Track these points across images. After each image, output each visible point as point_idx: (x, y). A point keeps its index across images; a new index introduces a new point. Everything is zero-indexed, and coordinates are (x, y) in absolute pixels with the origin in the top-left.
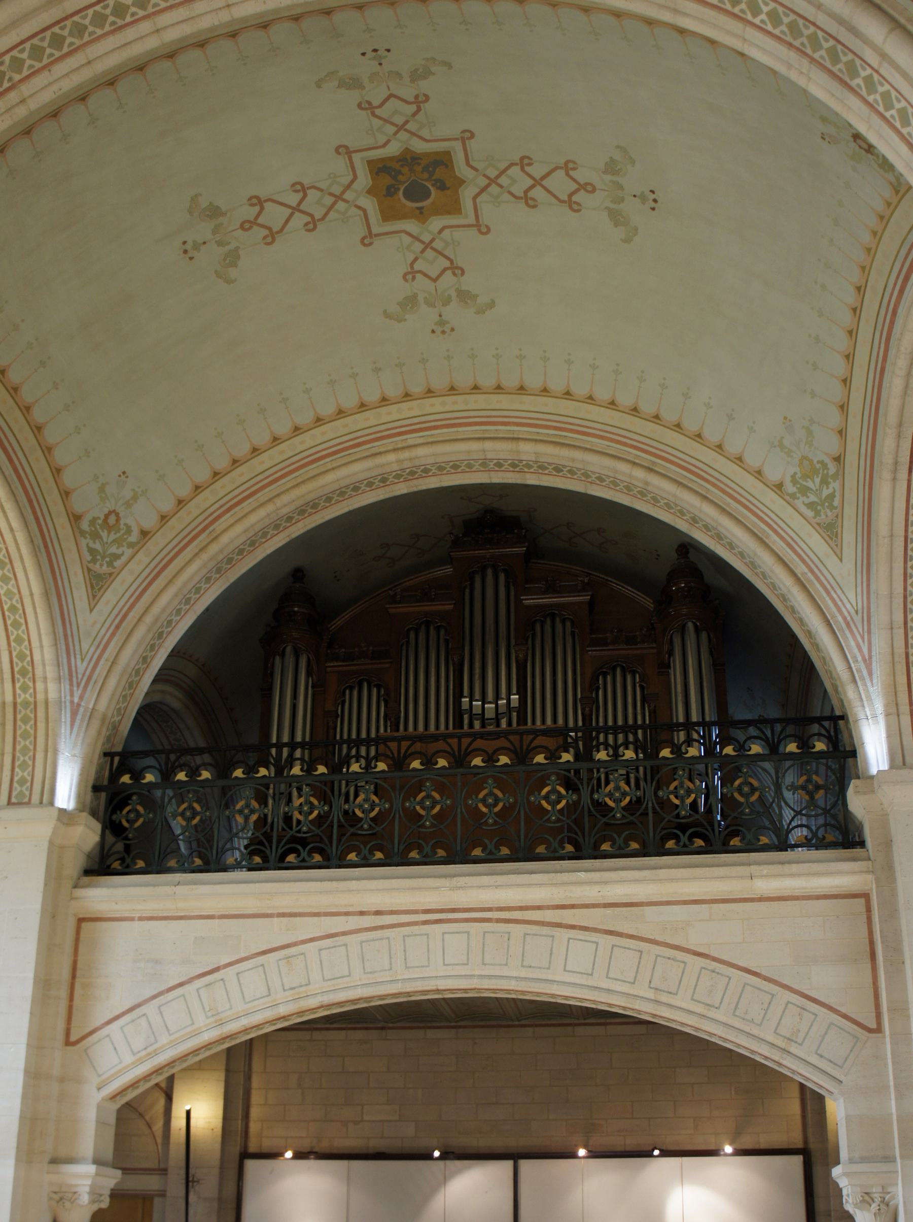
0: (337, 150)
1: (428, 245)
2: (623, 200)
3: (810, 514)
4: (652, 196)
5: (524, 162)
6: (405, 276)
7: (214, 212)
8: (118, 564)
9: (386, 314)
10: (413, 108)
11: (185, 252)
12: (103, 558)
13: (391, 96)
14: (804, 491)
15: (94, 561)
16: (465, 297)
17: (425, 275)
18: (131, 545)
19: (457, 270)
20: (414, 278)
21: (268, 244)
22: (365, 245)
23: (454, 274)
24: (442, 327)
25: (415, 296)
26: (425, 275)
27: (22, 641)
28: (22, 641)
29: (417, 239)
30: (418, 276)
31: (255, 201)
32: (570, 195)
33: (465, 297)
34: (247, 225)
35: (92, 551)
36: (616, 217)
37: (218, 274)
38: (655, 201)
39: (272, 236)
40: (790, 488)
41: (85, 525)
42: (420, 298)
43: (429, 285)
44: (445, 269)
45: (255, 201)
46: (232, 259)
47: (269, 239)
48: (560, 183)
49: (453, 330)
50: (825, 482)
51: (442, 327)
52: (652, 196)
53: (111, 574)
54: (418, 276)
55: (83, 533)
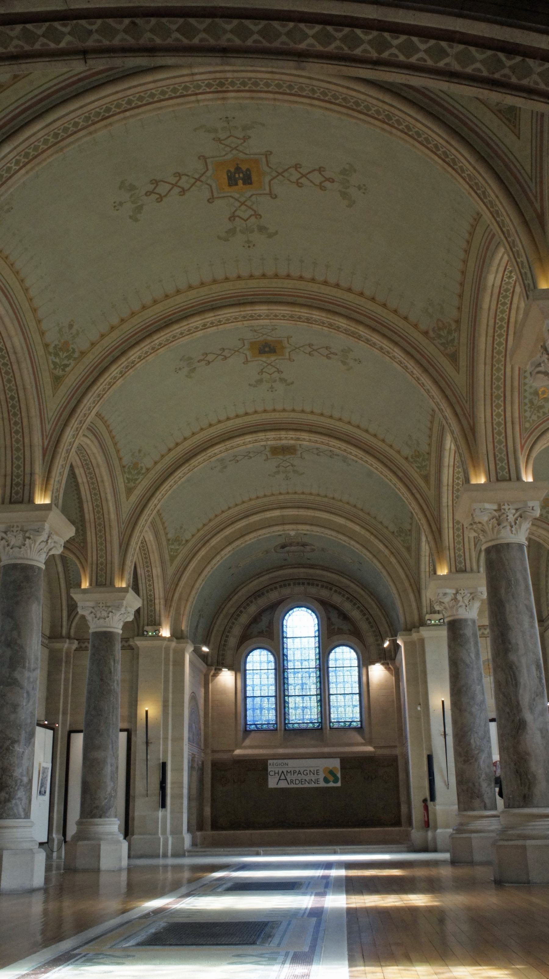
0: (199, 158)
1: (243, 204)
2: (349, 187)
3: (442, 348)
4: (364, 188)
5: (297, 167)
6: (230, 219)
7: (132, 188)
8: (67, 369)
9: (219, 237)
10: (242, 141)
11: (115, 207)
12: (60, 367)
13: (246, 220)
14: (440, 336)
15: (55, 368)
16: (262, 229)
17: (240, 218)
18: (75, 359)
19: (257, 215)
20: (234, 220)
21: (158, 202)
22: (211, 203)
23: (256, 218)
24: (249, 244)
25: (235, 228)
26: (240, 218)
27: (457, 536)
28: (457, 536)
29: (236, 200)
30: (237, 219)
31: (154, 182)
32: (321, 183)
33: (262, 229)
34: (148, 194)
35: (54, 363)
36: (344, 195)
37: (131, 217)
38: (365, 189)
39: (161, 198)
40: (431, 334)
41: (51, 349)
42: (238, 229)
43: (268, 376)
44: (251, 216)
45: (154, 182)
46: (139, 209)
47: (159, 200)
48: (317, 178)
49: (254, 245)
50: (450, 332)
51: (287, 478)
52: (364, 188)
53: (64, 376)
54: (237, 219)
55: (50, 354)
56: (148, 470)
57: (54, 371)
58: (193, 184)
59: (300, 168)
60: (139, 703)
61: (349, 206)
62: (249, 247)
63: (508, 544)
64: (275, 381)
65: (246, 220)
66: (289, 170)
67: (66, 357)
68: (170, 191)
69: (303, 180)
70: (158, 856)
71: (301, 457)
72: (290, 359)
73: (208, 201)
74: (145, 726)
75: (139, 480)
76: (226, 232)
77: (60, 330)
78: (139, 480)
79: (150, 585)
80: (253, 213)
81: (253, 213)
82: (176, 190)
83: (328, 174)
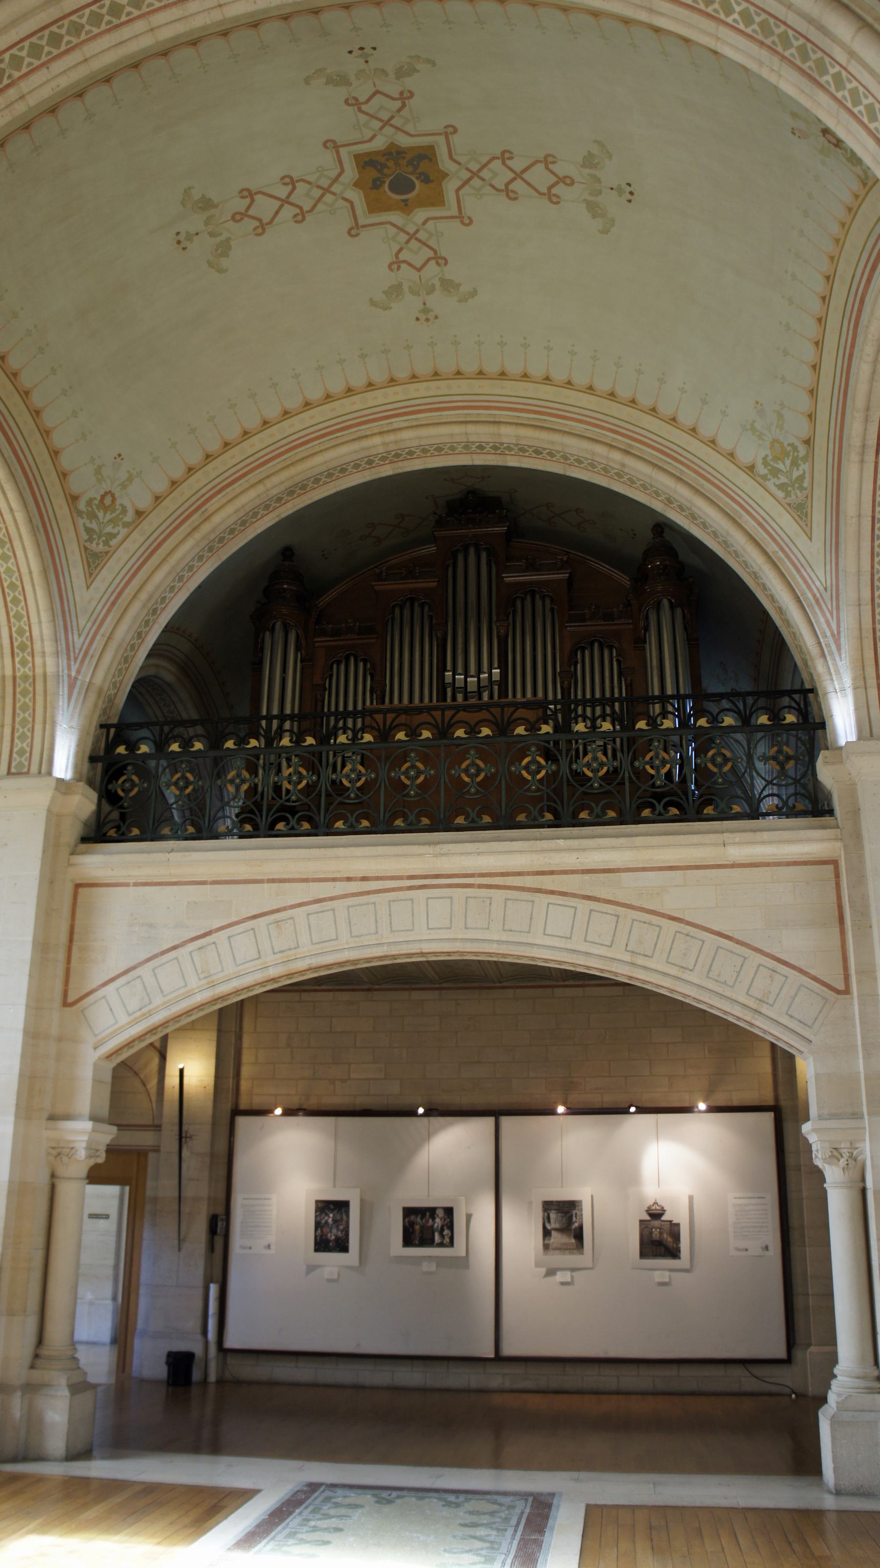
0: (325, 145)
1: (412, 236)
4: (629, 189)
5: (505, 156)
7: (206, 204)
8: (113, 542)
10: (398, 104)
11: (179, 242)
12: (99, 537)
13: (419, 270)
15: (90, 540)
16: (448, 285)
18: (126, 525)
19: (440, 260)
20: (399, 268)
22: (352, 236)
23: (438, 264)
24: (426, 315)
30: (403, 265)
31: (245, 193)
33: (448, 285)
35: (88, 530)
36: (594, 209)
37: (209, 263)
38: (631, 193)
39: (262, 227)
41: (82, 505)
42: (405, 288)
45: (245, 193)
46: (224, 249)
48: (540, 177)
49: (436, 317)
51: (426, 315)
52: (629, 189)
53: (107, 553)
55: (80, 513)
56: (139, 514)
57: (88, 544)
58: (319, 200)
59: (511, 158)
60: (211, 1097)
61: (605, 231)
62: (427, 320)
63: (546, 1561)
64: (431, 290)
65: (419, 270)
66: (491, 166)
67: (110, 521)
68: (277, 213)
69: (518, 186)
70: (40, 1458)
71: (460, 217)
72: (460, 217)
73: (349, 232)
74: (177, 1120)
75: (120, 538)
76: (385, 292)
77: (98, 471)
78: (120, 538)
79: (21, 632)
80: (432, 254)
81: (432, 254)
82: (288, 212)
83: (560, 169)
